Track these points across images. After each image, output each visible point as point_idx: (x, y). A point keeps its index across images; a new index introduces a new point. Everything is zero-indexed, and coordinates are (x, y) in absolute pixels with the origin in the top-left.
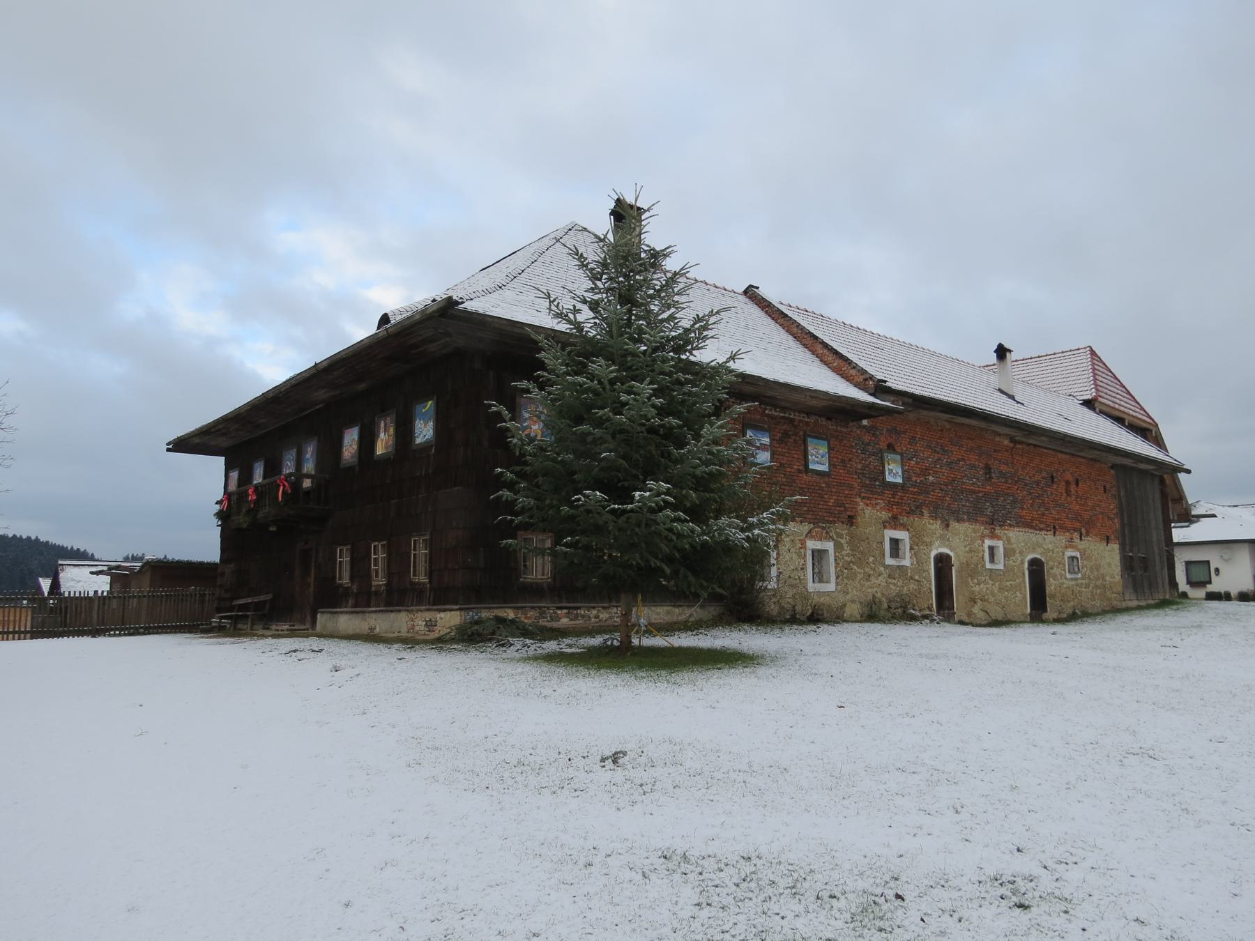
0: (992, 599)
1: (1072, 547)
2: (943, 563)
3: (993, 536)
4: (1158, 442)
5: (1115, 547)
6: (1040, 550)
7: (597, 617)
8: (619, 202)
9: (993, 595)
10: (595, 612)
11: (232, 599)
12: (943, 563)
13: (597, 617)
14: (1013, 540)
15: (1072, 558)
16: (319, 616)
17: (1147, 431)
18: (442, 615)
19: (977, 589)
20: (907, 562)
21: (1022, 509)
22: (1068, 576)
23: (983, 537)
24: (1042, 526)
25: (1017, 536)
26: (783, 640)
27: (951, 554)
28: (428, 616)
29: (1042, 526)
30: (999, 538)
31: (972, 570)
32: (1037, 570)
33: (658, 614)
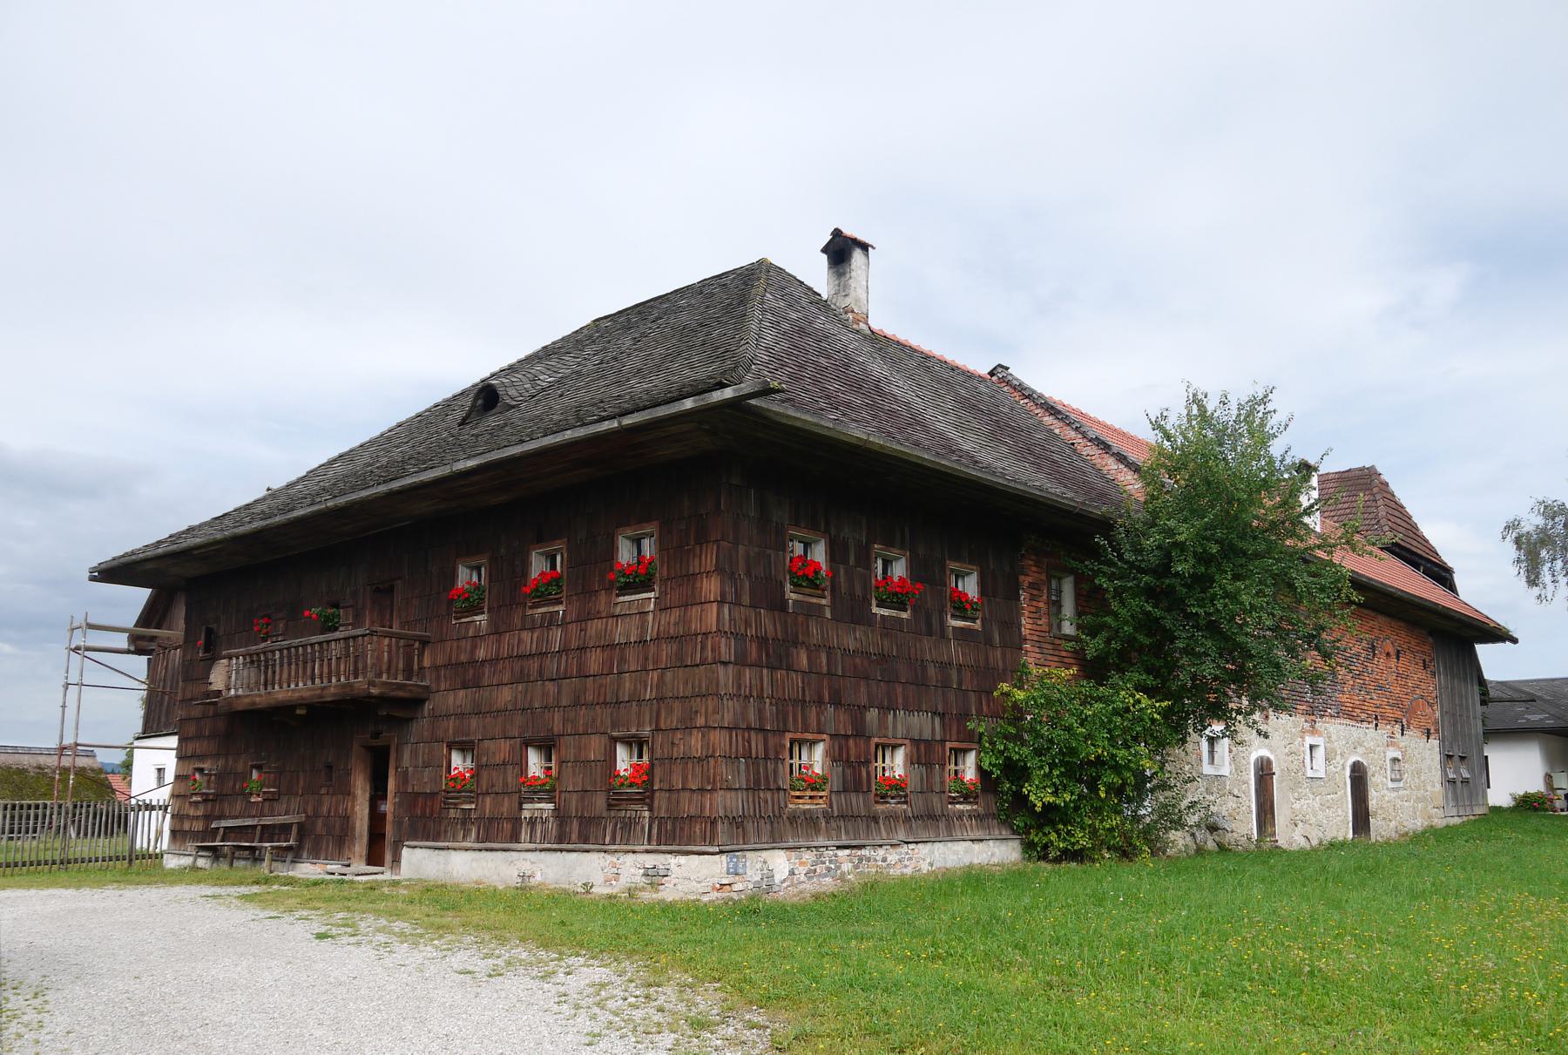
0: (1313, 820)
1: (1393, 744)
2: (1264, 773)
3: (1314, 731)
4: (1452, 587)
5: (1434, 743)
6: (1360, 750)
7: (884, 860)
8: (837, 233)
9: (1315, 815)
10: (881, 852)
11: (208, 818)
12: (1264, 773)
13: (884, 860)
14: (1334, 737)
15: (1395, 760)
16: (405, 852)
17: (1442, 575)
18: (682, 859)
19: (1297, 806)
20: (1226, 770)
21: (1343, 692)
22: (1391, 785)
23: (1303, 731)
24: (1363, 716)
25: (1335, 730)
26: (967, 861)
27: (1272, 757)
28: (650, 860)
29: (1363, 716)
30: (1320, 735)
31: (1297, 781)
32: (1359, 777)
33: (957, 853)
